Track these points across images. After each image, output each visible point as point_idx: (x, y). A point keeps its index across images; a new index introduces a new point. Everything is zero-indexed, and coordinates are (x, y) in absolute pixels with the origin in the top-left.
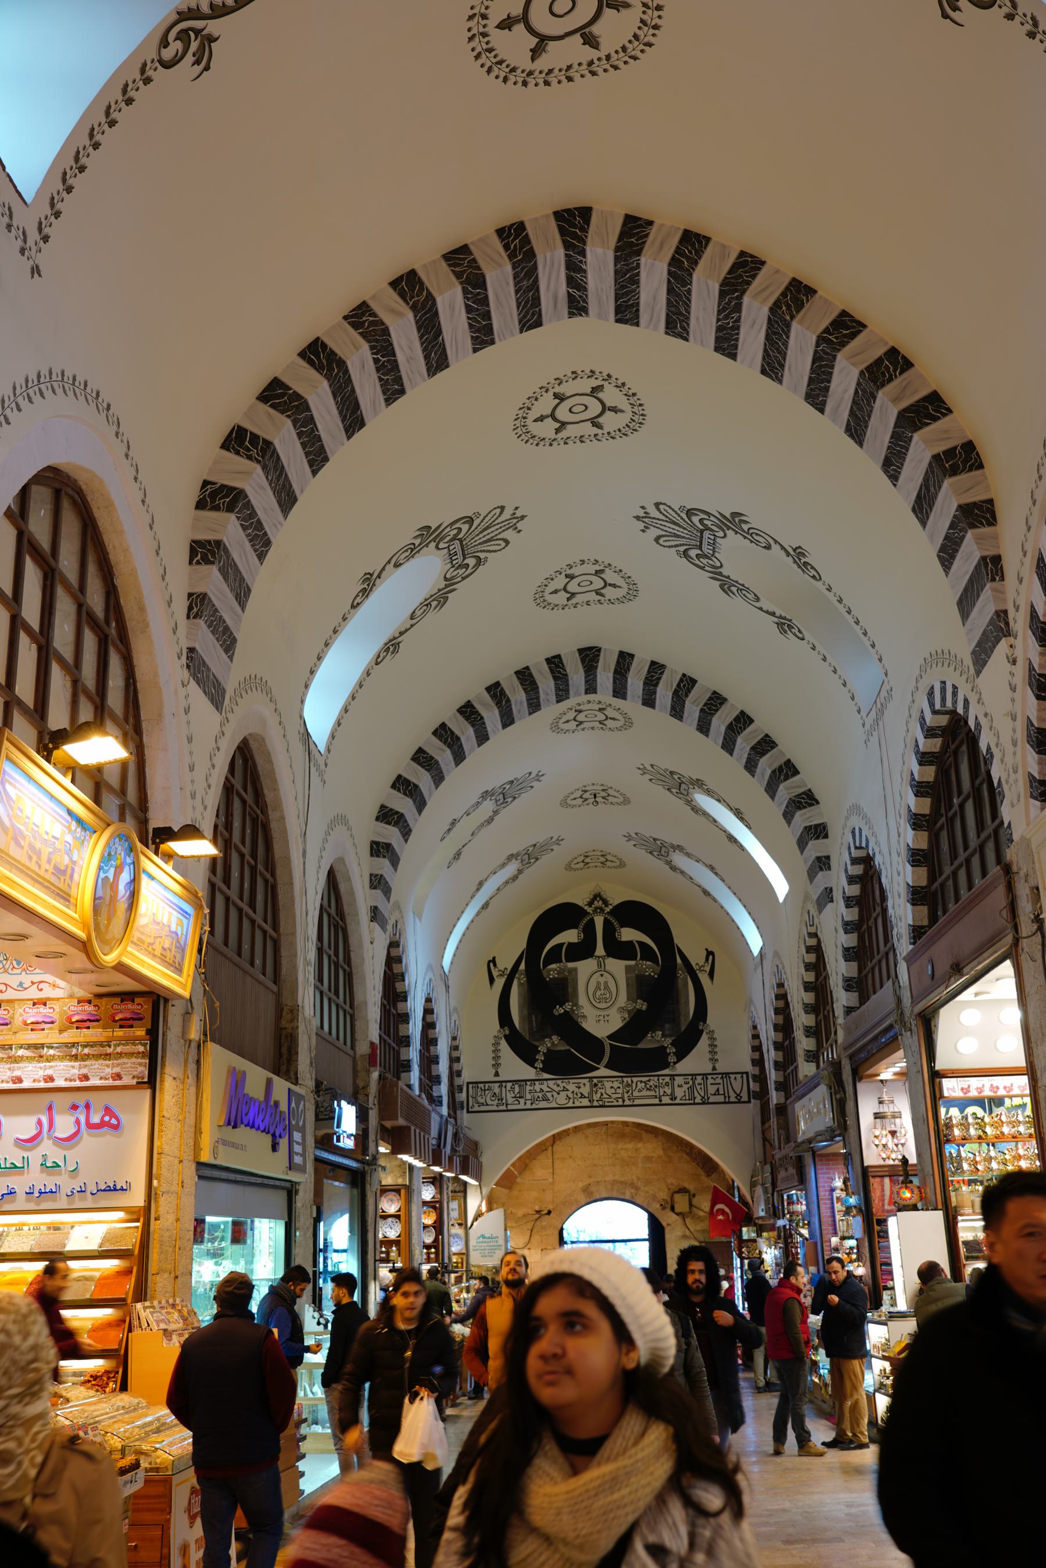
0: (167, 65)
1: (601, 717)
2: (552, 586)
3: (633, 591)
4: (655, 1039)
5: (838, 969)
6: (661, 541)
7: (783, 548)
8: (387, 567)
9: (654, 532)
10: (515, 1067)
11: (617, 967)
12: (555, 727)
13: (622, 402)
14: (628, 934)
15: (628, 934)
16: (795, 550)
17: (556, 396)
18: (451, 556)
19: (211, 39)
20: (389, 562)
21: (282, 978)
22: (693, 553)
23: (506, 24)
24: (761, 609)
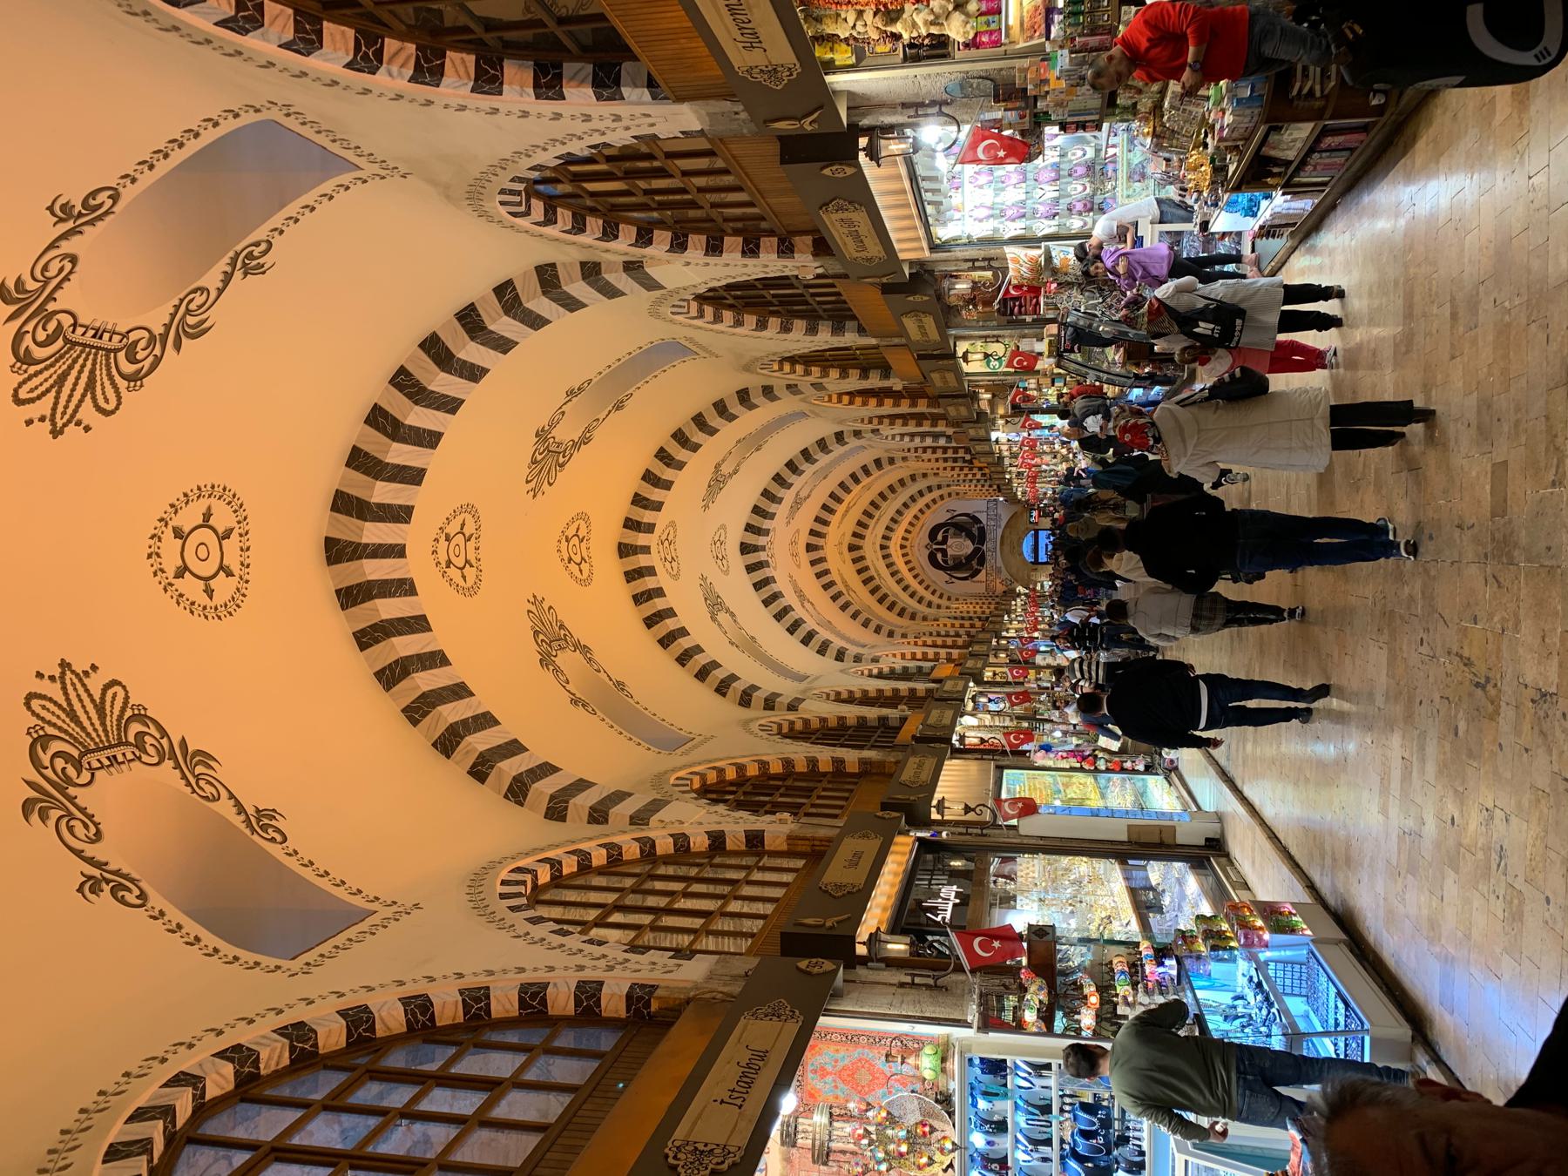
0: (285, 840)
1: (666, 543)
2: (459, 580)
3: (583, 517)
4: (975, 531)
5: (824, 339)
6: (110, 407)
7: (65, 236)
8: (88, 854)
9: (87, 412)
10: (982, 576)
11: (950, 541)
12: (676, 577)
13: (459, 519)
14: (940, 537)
15: (940, 537)
16: (61, 220)
17: (448, 567)
18: (559, 444)
19: (258, 811)
20: (78, 853)
21: (1366, 199)
22: (128, 368)
23: (209, 592)
24: (220, 291)
